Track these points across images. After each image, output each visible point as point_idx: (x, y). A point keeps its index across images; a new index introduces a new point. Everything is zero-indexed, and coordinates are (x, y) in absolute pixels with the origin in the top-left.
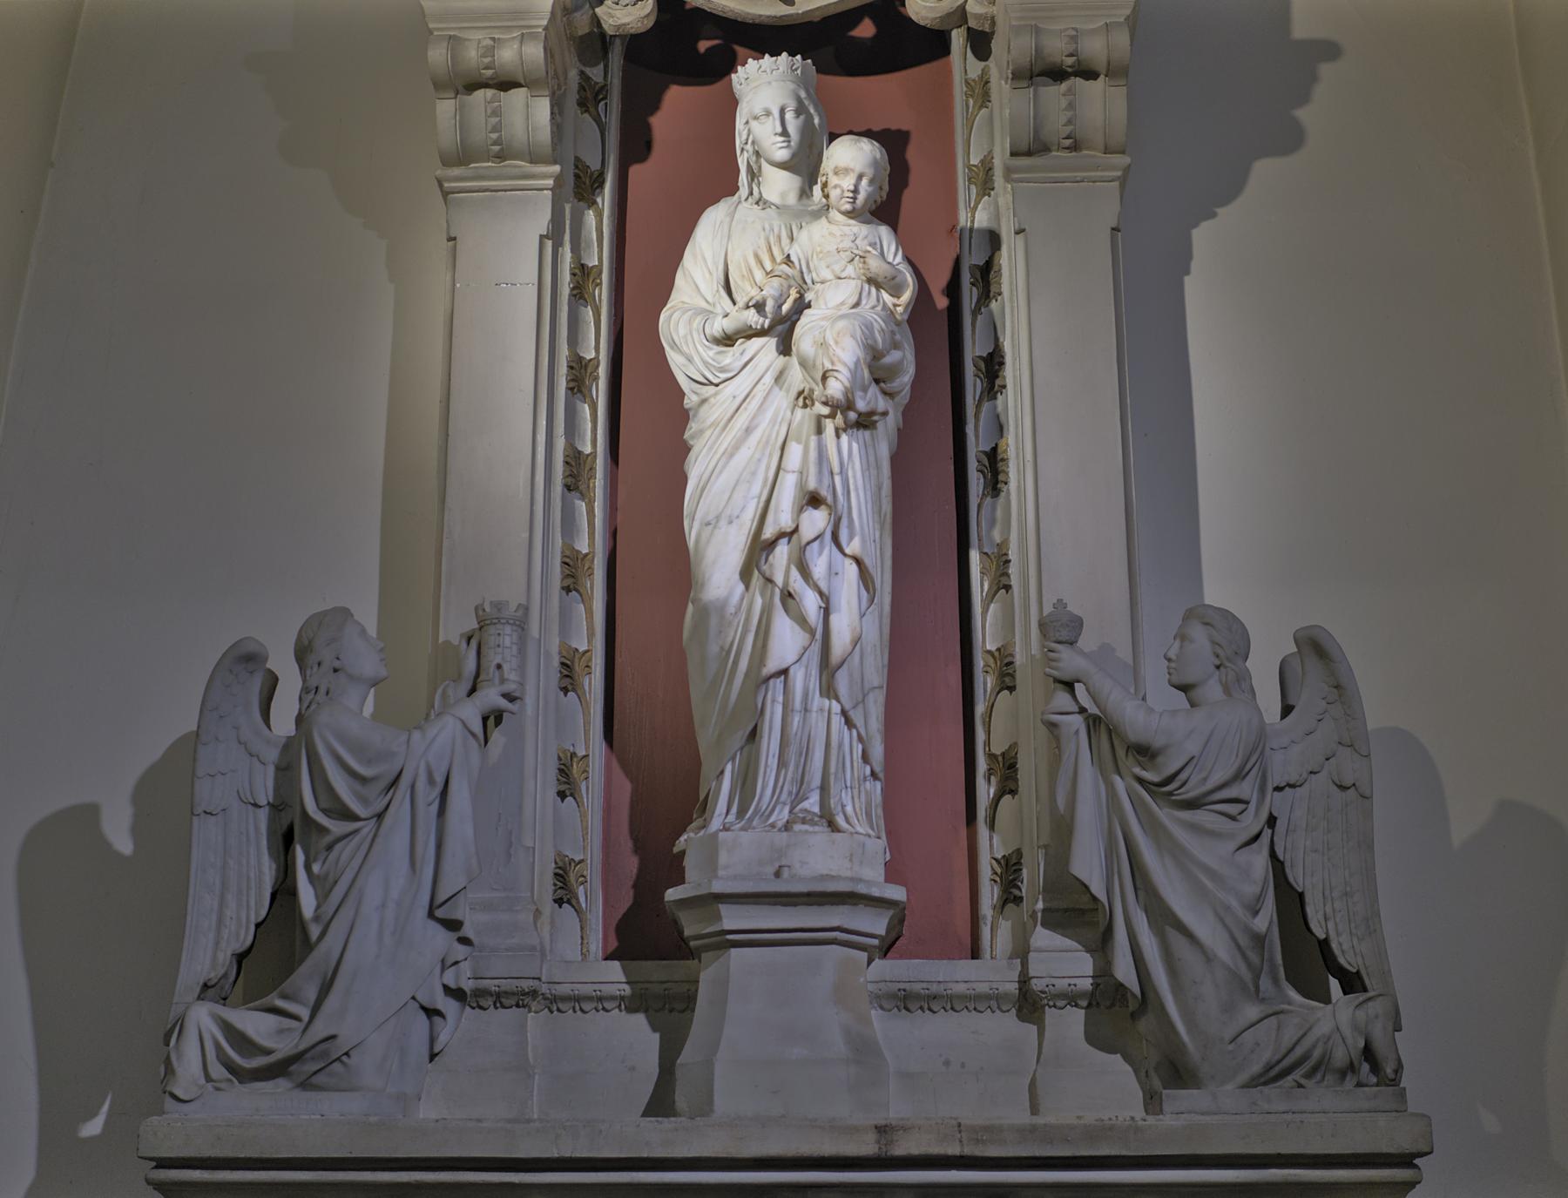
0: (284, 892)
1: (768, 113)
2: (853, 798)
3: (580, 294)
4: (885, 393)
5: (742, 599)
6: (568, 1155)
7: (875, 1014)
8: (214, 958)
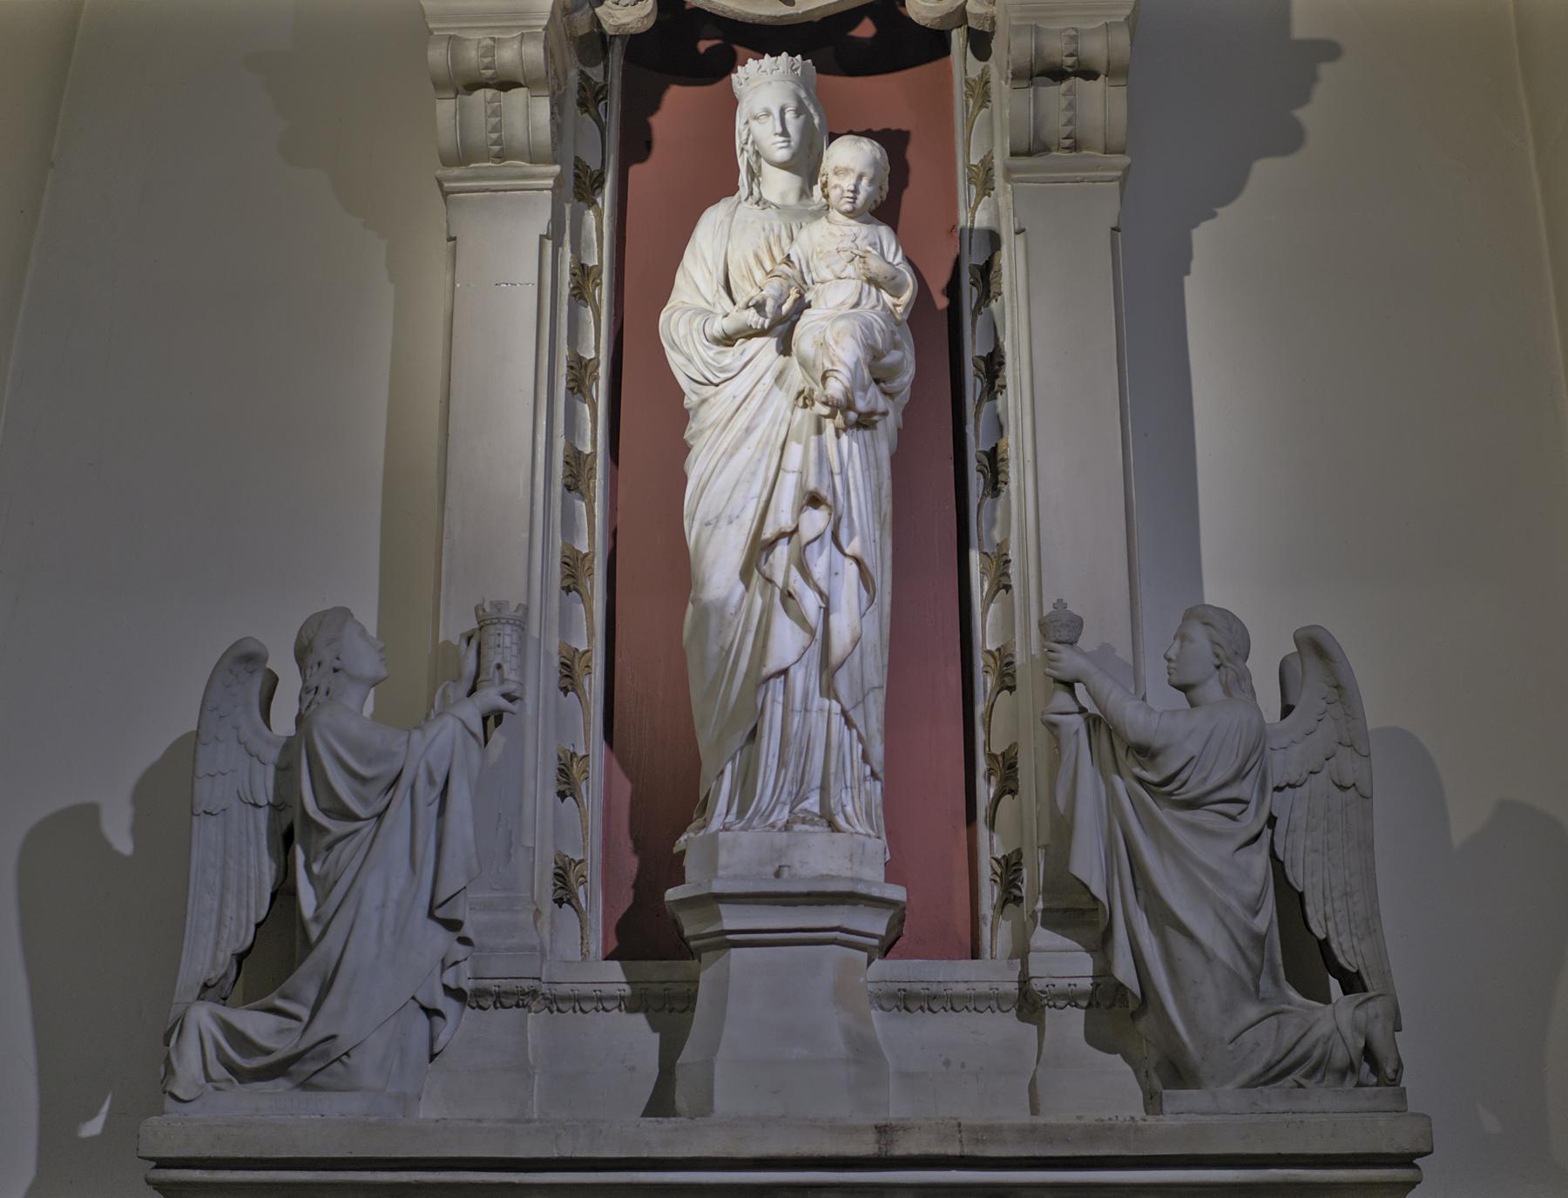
0: (284, 892)
1: (768, 113)
2: (853, 798)
3: (580, 294)
4: (885, 393)
5: (742, 599)
6: (568, 1155)
7: (875, 1014)
8: (214, 958)
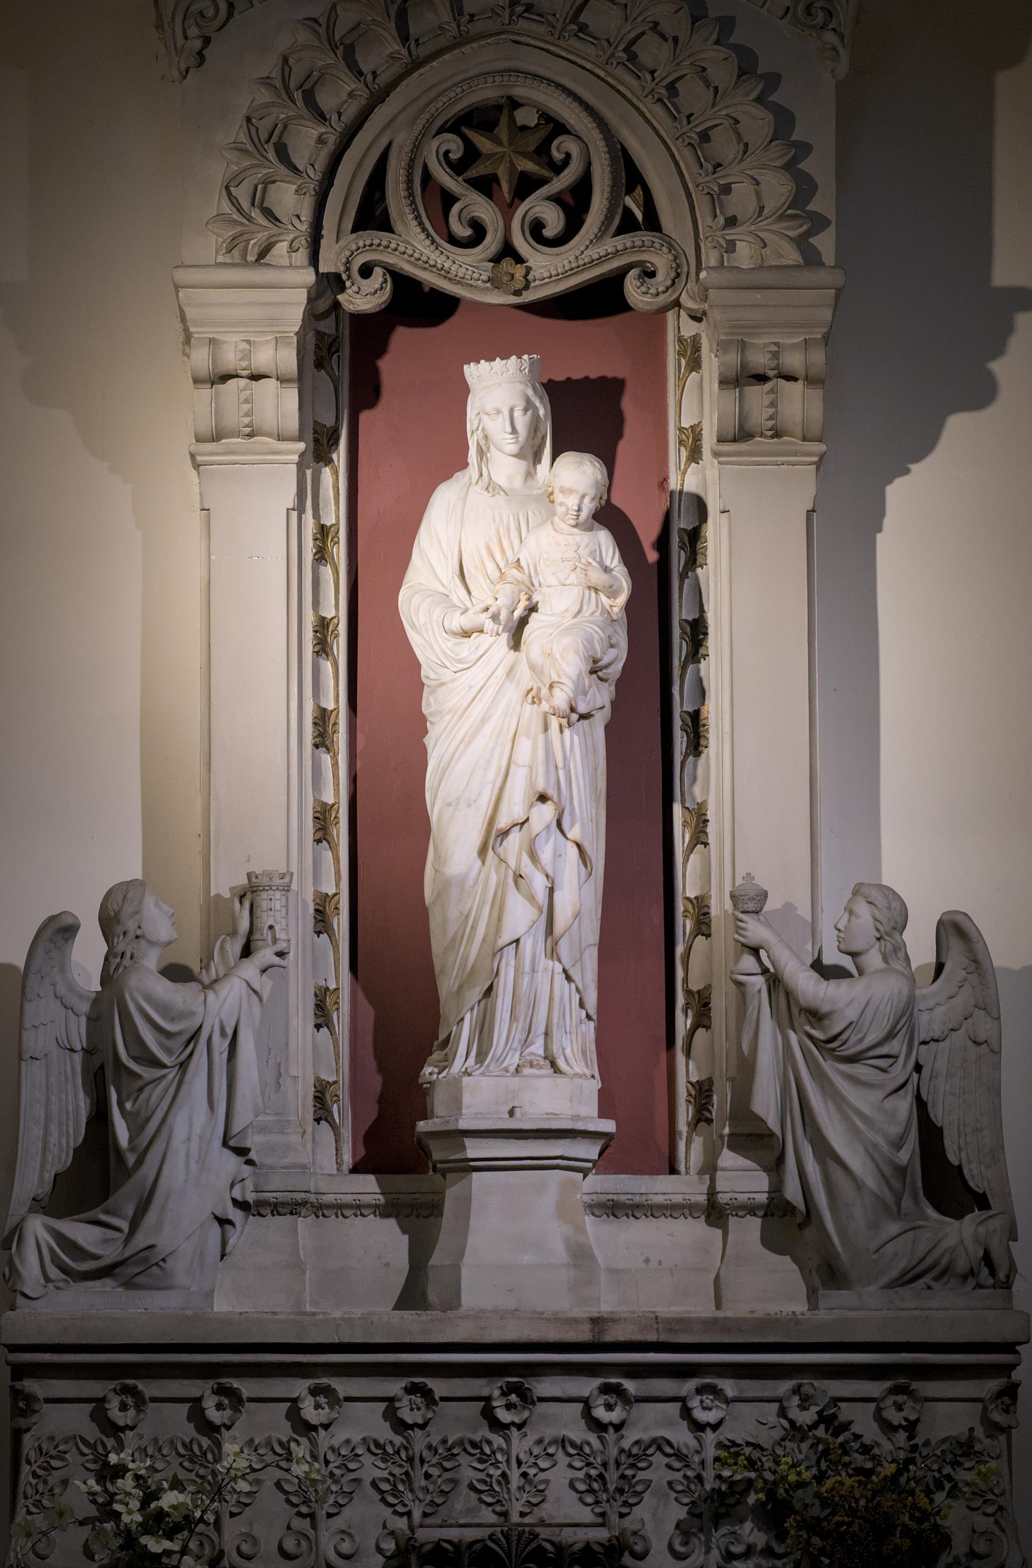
1: (498, 412)
2: (571, 1041)
3: (322, 556)
4: (601, 679)
5: (479, 873)
6: (346, 1341)
7: (589, 1220)
8: (41, 1176)
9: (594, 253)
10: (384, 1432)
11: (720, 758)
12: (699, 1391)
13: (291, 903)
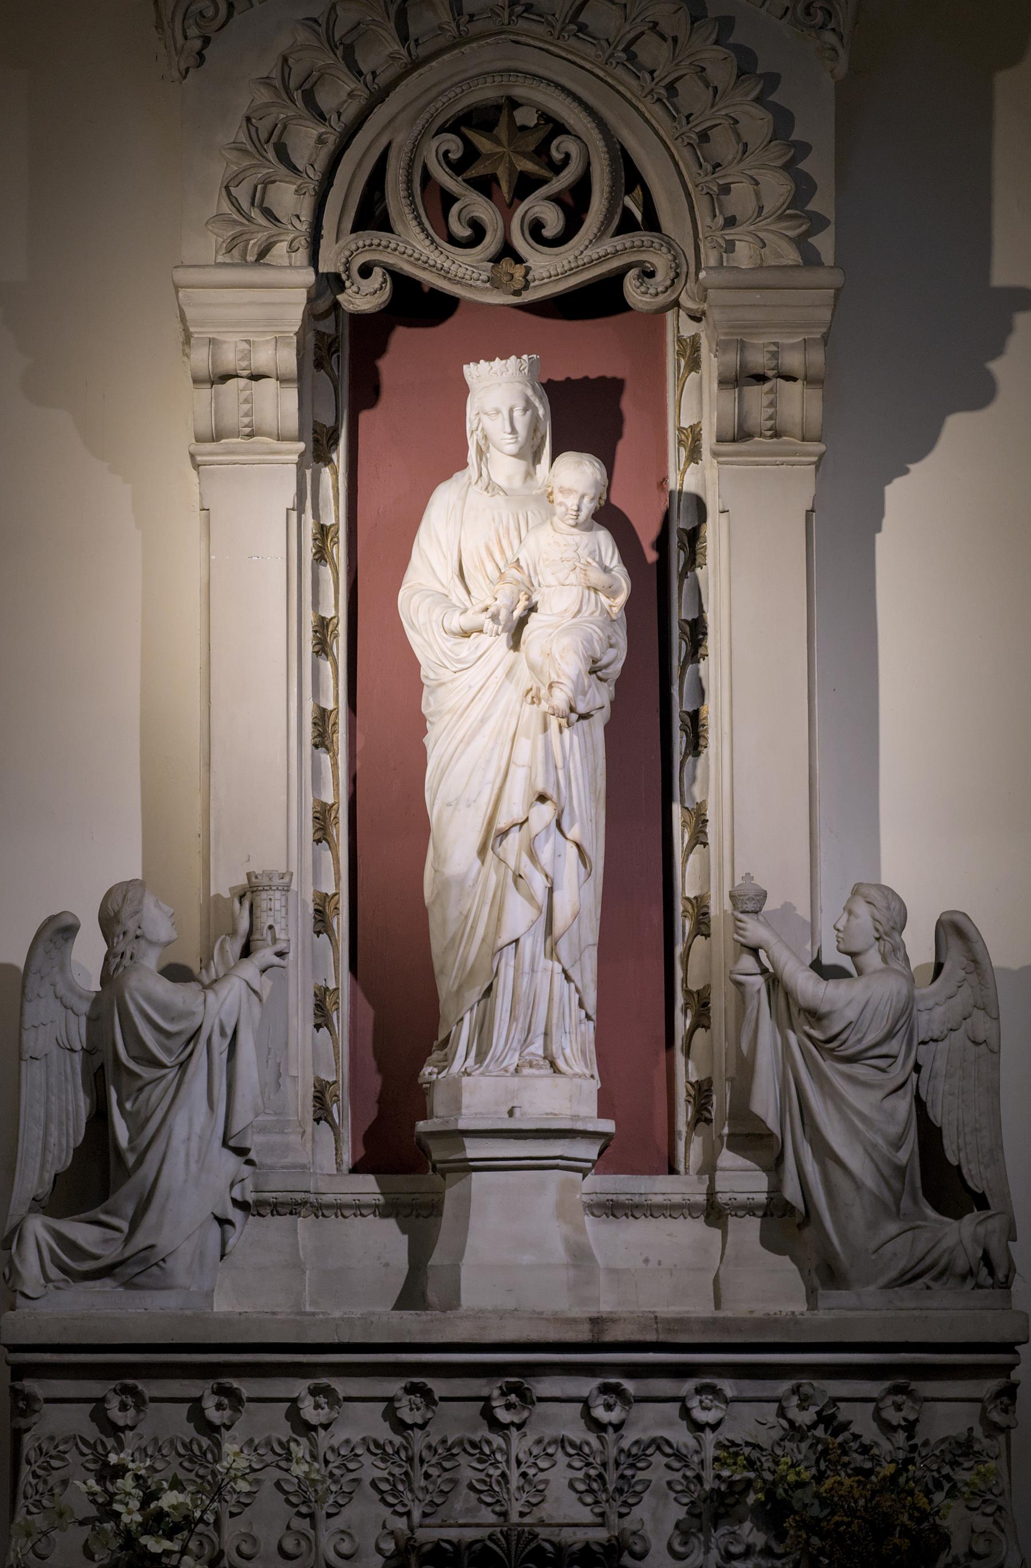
1: (498, 412)
2: (571, 1041)
3: (321, 556)
4: (600, 679)
5: (479, 873)
6: (346, 1341)
7: (588, 1220)
8: (41, 1176)
9: (594, 253)
10: (384, 1432)
11: (719, 758)
12: (699, 1391)
13: (291, 903)
